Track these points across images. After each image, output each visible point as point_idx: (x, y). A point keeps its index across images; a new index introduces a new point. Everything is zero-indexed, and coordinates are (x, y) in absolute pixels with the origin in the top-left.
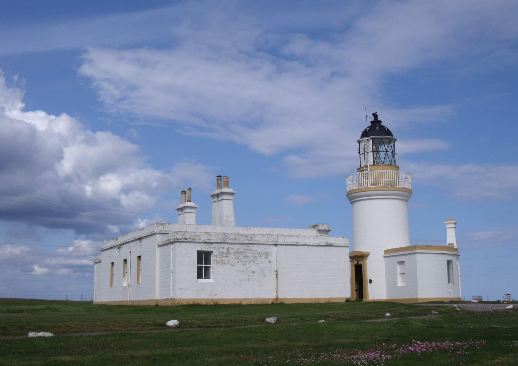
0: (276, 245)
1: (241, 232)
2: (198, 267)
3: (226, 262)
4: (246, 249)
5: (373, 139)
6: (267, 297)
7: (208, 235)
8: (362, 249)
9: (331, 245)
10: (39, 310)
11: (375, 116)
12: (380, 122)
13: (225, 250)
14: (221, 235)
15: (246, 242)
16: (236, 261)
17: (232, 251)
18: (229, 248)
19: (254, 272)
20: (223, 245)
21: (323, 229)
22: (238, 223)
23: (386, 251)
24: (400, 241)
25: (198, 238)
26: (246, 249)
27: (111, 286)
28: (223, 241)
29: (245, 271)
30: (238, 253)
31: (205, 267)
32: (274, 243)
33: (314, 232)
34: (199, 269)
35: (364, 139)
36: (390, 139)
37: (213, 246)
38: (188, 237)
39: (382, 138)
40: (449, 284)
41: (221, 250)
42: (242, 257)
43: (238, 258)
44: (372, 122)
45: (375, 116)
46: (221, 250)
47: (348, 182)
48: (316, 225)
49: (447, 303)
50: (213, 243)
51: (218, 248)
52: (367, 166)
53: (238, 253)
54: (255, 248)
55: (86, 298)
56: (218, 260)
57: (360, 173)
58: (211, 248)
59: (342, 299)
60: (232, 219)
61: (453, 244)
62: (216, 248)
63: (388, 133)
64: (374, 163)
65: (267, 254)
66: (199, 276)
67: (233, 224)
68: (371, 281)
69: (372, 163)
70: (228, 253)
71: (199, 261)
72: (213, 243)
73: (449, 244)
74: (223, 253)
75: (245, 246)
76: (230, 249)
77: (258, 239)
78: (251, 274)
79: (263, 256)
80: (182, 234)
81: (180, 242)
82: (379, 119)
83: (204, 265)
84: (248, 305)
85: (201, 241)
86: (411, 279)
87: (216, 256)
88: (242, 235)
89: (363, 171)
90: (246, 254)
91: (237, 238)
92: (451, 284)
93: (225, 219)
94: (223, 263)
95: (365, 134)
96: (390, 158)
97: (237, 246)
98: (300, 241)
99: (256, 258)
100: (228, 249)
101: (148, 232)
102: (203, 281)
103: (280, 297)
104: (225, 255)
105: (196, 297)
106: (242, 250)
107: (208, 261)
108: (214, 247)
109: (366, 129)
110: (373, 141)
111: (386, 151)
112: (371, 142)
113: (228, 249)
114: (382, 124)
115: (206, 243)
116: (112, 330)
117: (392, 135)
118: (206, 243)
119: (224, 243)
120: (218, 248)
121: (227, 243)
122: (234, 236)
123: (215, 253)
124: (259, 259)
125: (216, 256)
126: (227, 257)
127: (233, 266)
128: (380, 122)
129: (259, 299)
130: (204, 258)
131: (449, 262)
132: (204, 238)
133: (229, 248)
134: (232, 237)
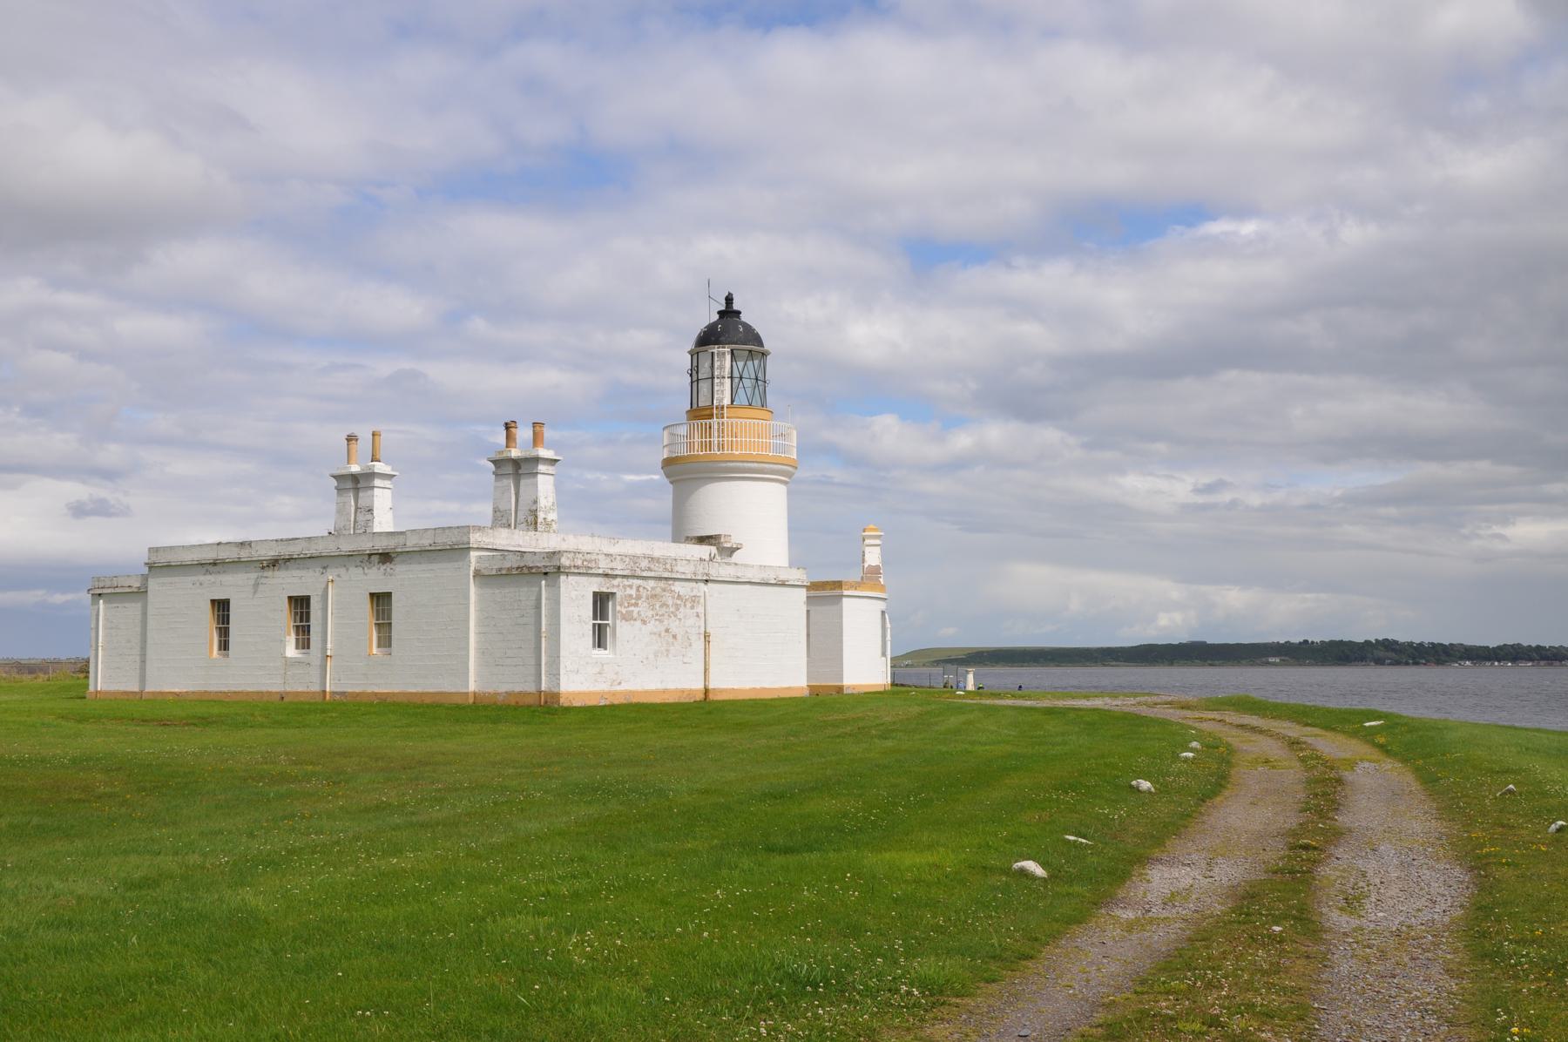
1: (657, 554)
6: (687, 686)
9: (783, 584)
11: (729, 300)
13: (633, 592)
16: (650, 613)
17: (644, 593)
20: (631, 581)
27: (224, 646)
37: (616, 582)
38: (579, 563)
41: (629, 591)
46: (629, 591)
50: (616, 576)
54: (678, 587)
70: (639, 597)
72: (616, 576)
75: (662, 584)
77: (681, 569)
82: (736, 307)
89: (711, 416)
93: (541, 516)
94: (628, 617)
96: (749, 391)
97: (652, 583)
99: (677, 607)
102: (602, 651)
106: (658, 590)
115: (606, 575)
117: (760, 343)
118: (606, 575)
119: (634, 577)
121: (638, 577)
123: (618, 596)
126: (636, 605)
129: (683, 691)
130: (601, 602)
132: (604, 565)
134: (644, 564)
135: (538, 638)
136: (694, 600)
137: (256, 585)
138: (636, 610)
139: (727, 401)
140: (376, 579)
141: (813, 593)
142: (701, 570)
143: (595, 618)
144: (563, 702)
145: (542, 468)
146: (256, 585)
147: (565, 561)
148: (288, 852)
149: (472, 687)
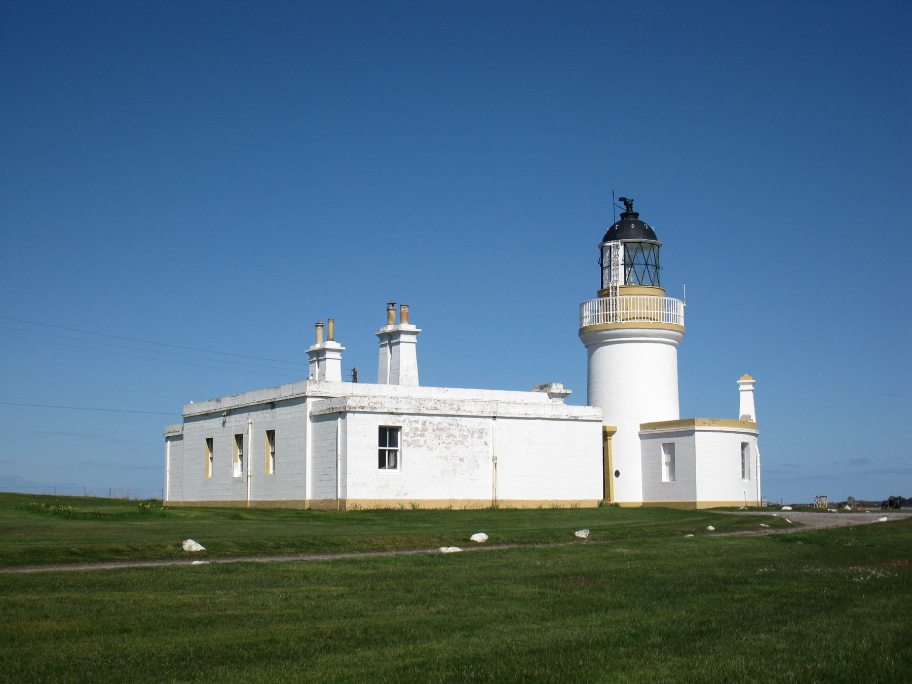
0: (495, 417)
2: (380, 450)
3: (421, 443)
4: (450, 425)
5: (625, 244)
6: (481, 498)
7: (394, 401)
8: (609, 424)
9: (576, 420)
10: (246, 519)
12: (636, 215)
13: (420, 426)
14: (413, 402)
15: (451, 413)
16: (436, 442)
17: (430, 427)
18: (425, 422)
19: (462, 460)
20: (417, 417)
21: (558, 391)
22: (425, 381)
23: (643, 426)
24: (668, 410)
25: (379, 405)
26: (450, 425)
28: (417, 411)
29: (449, 458)
30: (438, 429)
31: (389, 451)
32: (492, 415)
33: (544, 395)
34: (382, 454)
35: (611, 244)
36: (652, 244)
38: (366, 404)
39: (640, 243)
40: (744, 480)
41: (415, 425)
42: (444, 435)
43: (439, 437)
44: (623, 215)
45: (628, 204)
47: (587, 313)
48: (546, 386)
49: (743, 510)
50: (402, 414)
51: (410, 422)
52: (616, 288)
53: (438, 429)
55: (137, 490)
56: (410, 440)
57: (602, 299)
58: (399, 421)
59: (592, 501)
60: (415, 373)
61: (749, 417)
62: (407, 422)
63: (650, 234)
64: (625, 283)
65: (481, 432)
66: (382, 465)
67: (416, 381)
68: (617, 474)
69: (623, 283)
71: (382, 442)
72: (402, 414)
73: (743, 416)
74: (417, 429)
75: (449, 419)
76: (427, 424)
77: (468, 409)
78: (458, 462)
79: (476, 435)
80: (357, 399)
81: (354, 412)
82: (635, 210)
83: (388, 448)
84: (461, 510)
85: (385, 410)
86: (682, 467)
87: (407, 435)
88: (445, 402)
89: (608, 295)
90: (451, 432)
91: (438, 407)
92: (746, 480)
95: (611, 235)
98: (532, 413)
99: (465, 437)
100: (424, 423)
101: (290, 393)
102: (386, 471)
103: (499, 498)
104: (419, 433)
105: (377, 498)
106: (445, 425)
107: (394, 442)
108: (404, 421)
109: (613, 227)
110: (625, 246)
111: (647, 264)
112: (622, 248)
113: (424, 423)
114: (640, 218)
115: (392, 413)
116: (21, 541)
118: (392, 413)
120: (410, 422)
122: (433, 402)
123: (406, 429)
124: (469, 439)
125: (407, 435)
127: (431, 449)
128: (636, 215)
129: (469, 501)
130: (388, 435)
131: (744, 445)
133: (425, 422)
134: (430, 404)
135: (332, 459)
136: (481, 432)
137: (224, 423)
138: (422, 439)
139: (621, 282)
140: (266, 419)
141: (690, 428)
142: (489, 408)
143: (380, 446)
144: (699, 507)
145: (403, 338)
146: (224, 423)
147: (351, 403)
148: (647, 610)
149: (309, 496)
